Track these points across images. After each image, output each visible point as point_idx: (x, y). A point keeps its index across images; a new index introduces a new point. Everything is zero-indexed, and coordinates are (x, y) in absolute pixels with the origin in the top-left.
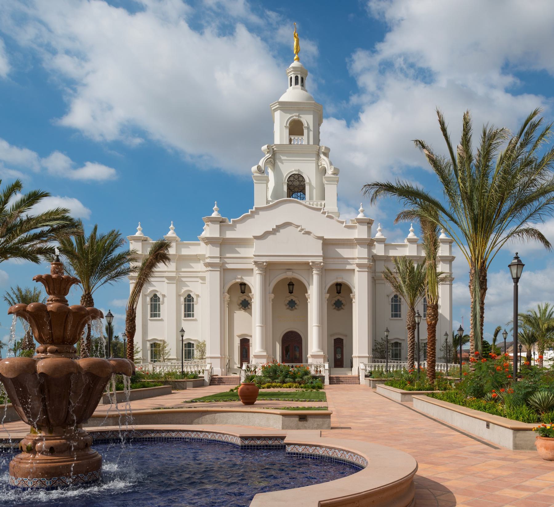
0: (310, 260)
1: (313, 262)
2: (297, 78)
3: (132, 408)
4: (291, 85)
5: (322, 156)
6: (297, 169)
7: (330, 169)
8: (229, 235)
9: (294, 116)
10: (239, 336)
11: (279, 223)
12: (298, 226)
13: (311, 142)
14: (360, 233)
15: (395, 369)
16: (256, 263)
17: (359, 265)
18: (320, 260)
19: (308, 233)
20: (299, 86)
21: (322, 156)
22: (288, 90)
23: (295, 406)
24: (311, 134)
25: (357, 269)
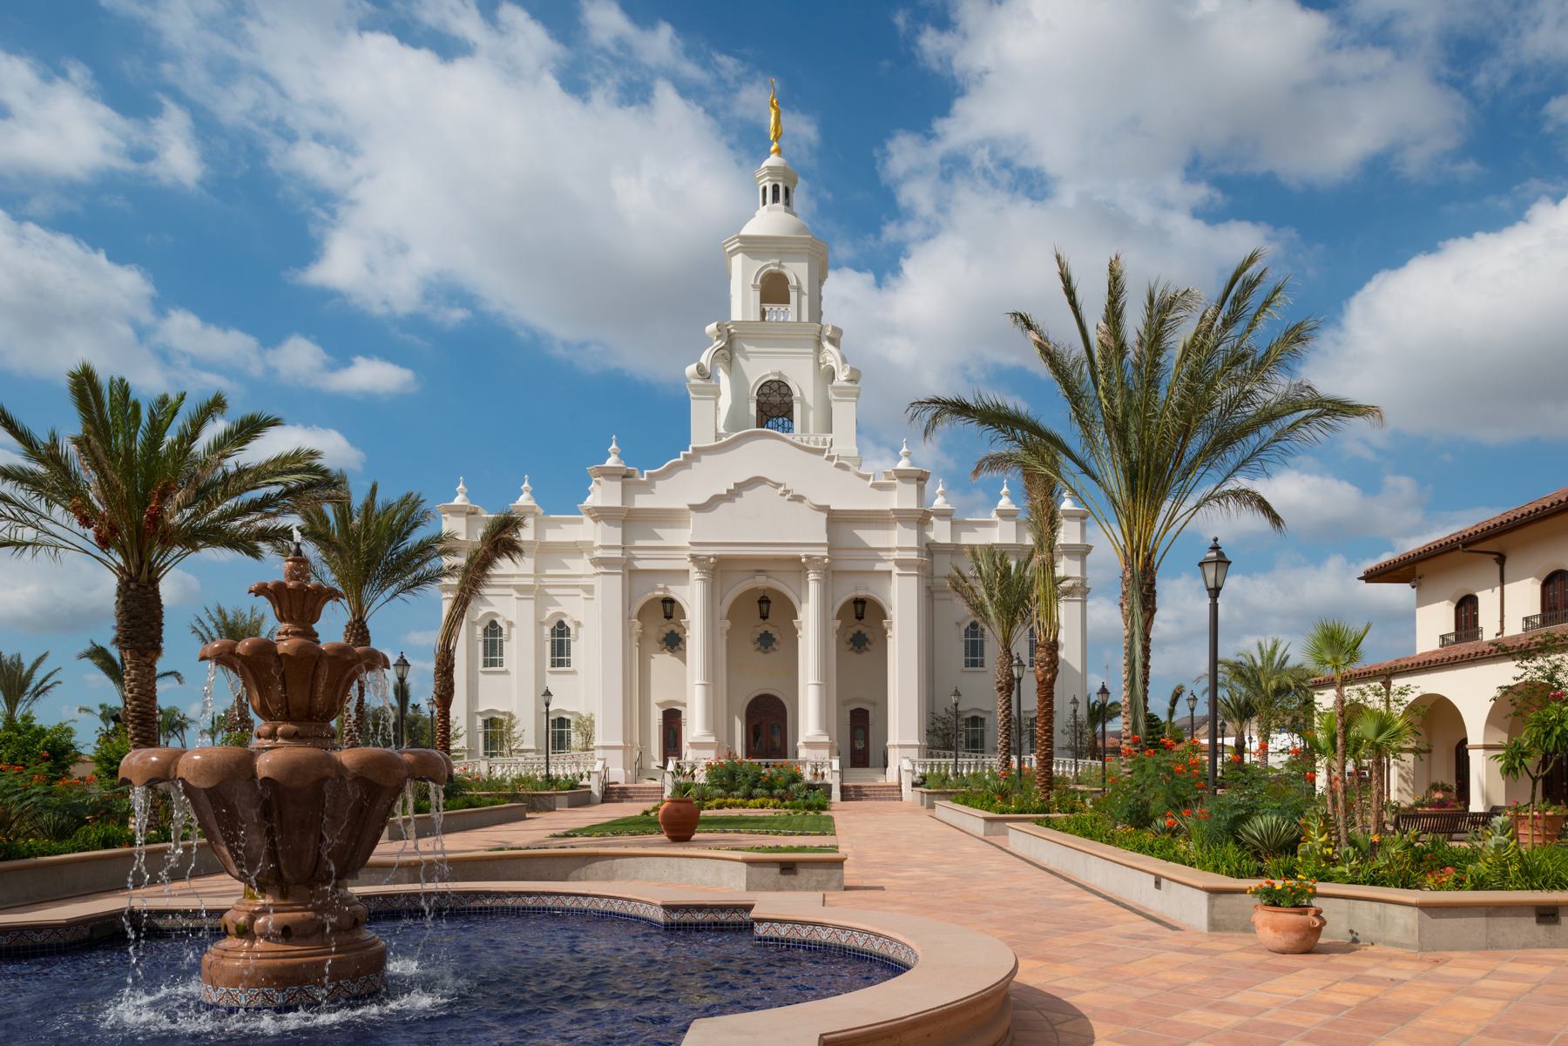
0: (802, 552)
1: (808, 557)
2: (776, 188)
5: (826, 344)
6: (776, 370)
9: (772, 264)
10: (660, 705)
12: (778, 485)
14: (902, 498)
16: (694, 558)
17: (900, 563)
18: (823, 552)
19: (799, 498)
21: (826, 344)
23: (773, 844)
24: (805, 300)
25: (896, 570)
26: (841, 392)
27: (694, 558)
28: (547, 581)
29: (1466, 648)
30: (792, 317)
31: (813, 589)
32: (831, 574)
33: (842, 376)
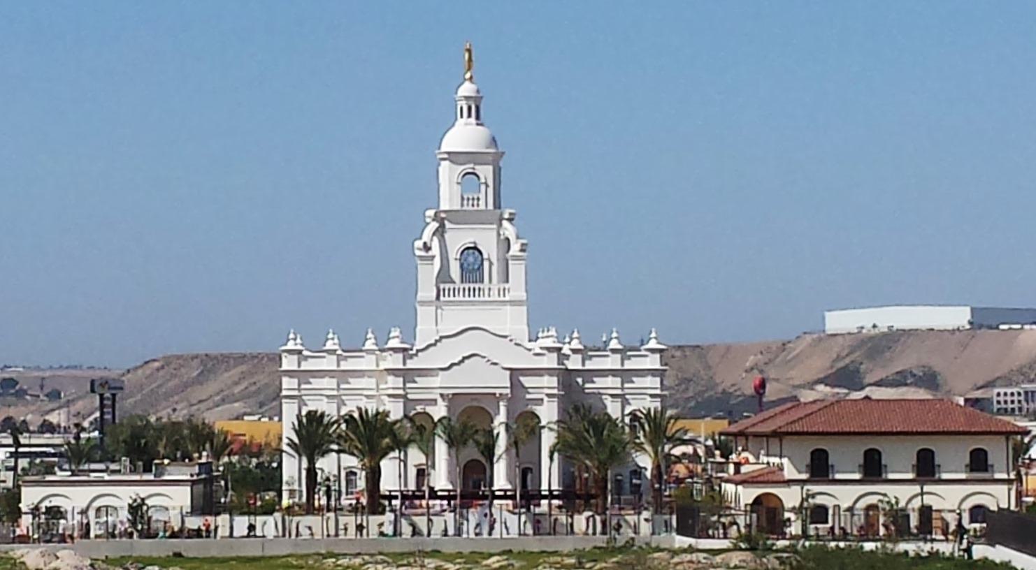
0: (498, 391)
1: (501, 394)
2: (470, 109)
3: (1029, 477)
4: (462, 116)
5: (505, 223)
6: (472, 240)
7: (516, 243)
8: (411, 364)
9: (468, 167)
10: (415, 466)
11: (466, 354)
12: (484, 357)
13: (491, 207)
14: (550, 361)
15: (823, 419)
16: (442, 395)
17: (548, 395)
18: (508, 391)
19: (495, 364)
20: (473, 120)
21: (505, 223)
22: (457, 123)
23: (762, 419)
24: (490, 190)
25: (546, 399)
26: (516, 258)
27: (442, 395)
28: (342, 392)
29: (873, 444)
30: (482, 207)
31: (503, 410)
32: (511, 401)
33: (515, 248)
